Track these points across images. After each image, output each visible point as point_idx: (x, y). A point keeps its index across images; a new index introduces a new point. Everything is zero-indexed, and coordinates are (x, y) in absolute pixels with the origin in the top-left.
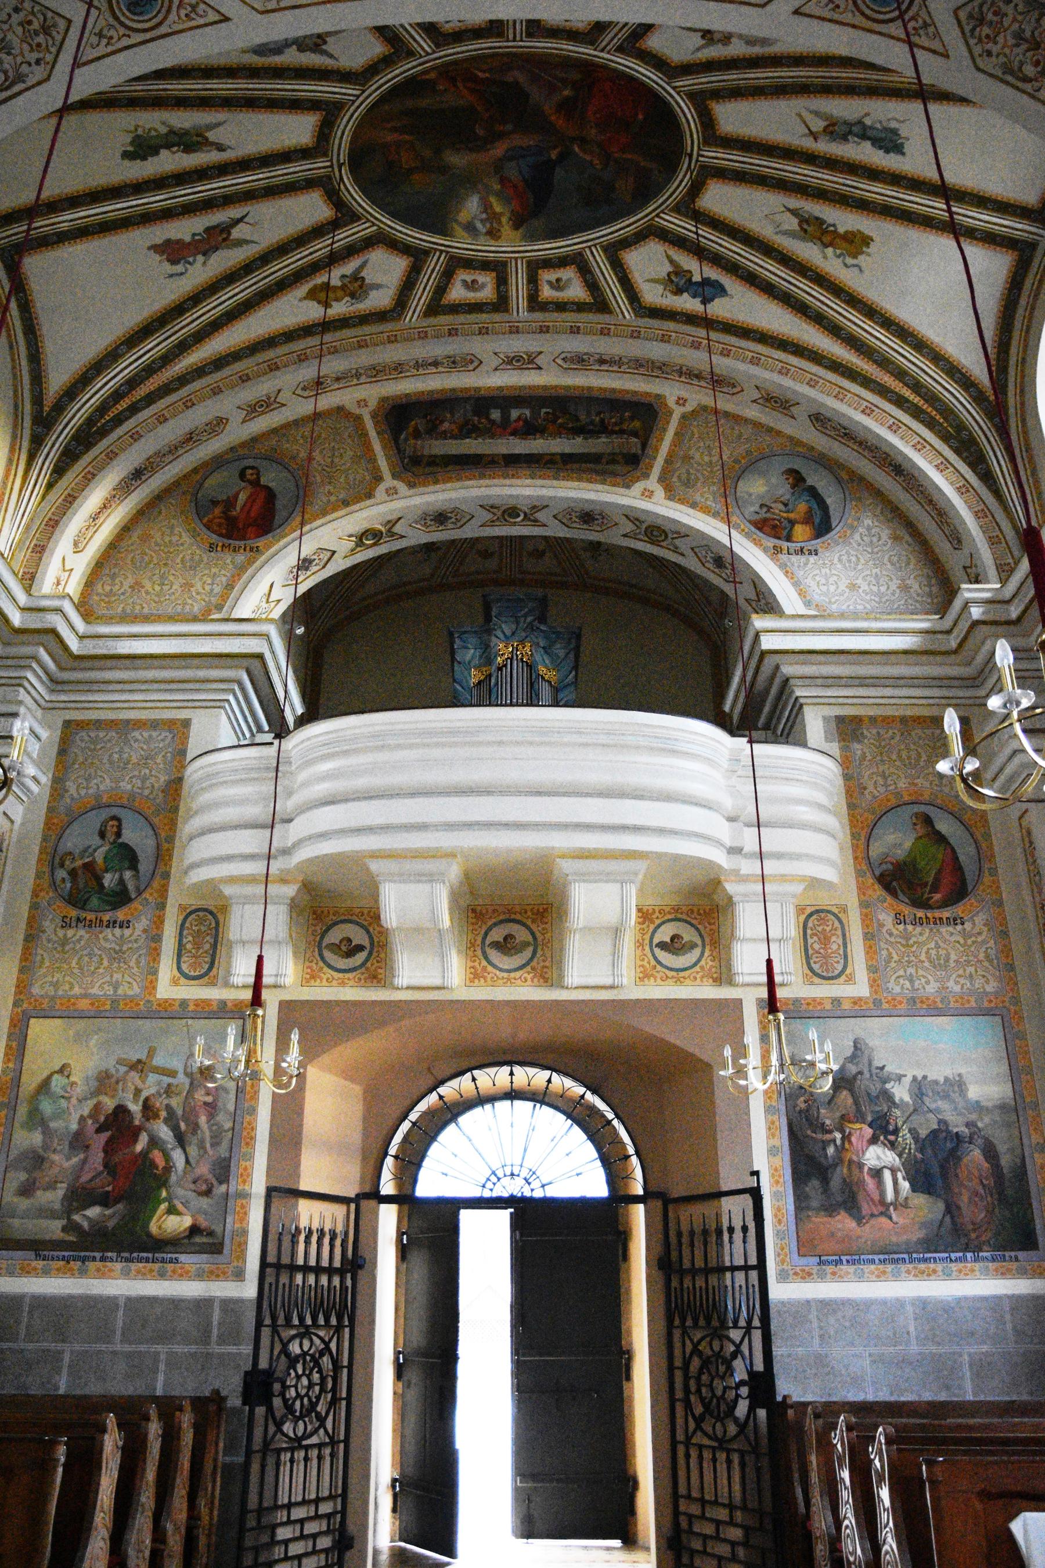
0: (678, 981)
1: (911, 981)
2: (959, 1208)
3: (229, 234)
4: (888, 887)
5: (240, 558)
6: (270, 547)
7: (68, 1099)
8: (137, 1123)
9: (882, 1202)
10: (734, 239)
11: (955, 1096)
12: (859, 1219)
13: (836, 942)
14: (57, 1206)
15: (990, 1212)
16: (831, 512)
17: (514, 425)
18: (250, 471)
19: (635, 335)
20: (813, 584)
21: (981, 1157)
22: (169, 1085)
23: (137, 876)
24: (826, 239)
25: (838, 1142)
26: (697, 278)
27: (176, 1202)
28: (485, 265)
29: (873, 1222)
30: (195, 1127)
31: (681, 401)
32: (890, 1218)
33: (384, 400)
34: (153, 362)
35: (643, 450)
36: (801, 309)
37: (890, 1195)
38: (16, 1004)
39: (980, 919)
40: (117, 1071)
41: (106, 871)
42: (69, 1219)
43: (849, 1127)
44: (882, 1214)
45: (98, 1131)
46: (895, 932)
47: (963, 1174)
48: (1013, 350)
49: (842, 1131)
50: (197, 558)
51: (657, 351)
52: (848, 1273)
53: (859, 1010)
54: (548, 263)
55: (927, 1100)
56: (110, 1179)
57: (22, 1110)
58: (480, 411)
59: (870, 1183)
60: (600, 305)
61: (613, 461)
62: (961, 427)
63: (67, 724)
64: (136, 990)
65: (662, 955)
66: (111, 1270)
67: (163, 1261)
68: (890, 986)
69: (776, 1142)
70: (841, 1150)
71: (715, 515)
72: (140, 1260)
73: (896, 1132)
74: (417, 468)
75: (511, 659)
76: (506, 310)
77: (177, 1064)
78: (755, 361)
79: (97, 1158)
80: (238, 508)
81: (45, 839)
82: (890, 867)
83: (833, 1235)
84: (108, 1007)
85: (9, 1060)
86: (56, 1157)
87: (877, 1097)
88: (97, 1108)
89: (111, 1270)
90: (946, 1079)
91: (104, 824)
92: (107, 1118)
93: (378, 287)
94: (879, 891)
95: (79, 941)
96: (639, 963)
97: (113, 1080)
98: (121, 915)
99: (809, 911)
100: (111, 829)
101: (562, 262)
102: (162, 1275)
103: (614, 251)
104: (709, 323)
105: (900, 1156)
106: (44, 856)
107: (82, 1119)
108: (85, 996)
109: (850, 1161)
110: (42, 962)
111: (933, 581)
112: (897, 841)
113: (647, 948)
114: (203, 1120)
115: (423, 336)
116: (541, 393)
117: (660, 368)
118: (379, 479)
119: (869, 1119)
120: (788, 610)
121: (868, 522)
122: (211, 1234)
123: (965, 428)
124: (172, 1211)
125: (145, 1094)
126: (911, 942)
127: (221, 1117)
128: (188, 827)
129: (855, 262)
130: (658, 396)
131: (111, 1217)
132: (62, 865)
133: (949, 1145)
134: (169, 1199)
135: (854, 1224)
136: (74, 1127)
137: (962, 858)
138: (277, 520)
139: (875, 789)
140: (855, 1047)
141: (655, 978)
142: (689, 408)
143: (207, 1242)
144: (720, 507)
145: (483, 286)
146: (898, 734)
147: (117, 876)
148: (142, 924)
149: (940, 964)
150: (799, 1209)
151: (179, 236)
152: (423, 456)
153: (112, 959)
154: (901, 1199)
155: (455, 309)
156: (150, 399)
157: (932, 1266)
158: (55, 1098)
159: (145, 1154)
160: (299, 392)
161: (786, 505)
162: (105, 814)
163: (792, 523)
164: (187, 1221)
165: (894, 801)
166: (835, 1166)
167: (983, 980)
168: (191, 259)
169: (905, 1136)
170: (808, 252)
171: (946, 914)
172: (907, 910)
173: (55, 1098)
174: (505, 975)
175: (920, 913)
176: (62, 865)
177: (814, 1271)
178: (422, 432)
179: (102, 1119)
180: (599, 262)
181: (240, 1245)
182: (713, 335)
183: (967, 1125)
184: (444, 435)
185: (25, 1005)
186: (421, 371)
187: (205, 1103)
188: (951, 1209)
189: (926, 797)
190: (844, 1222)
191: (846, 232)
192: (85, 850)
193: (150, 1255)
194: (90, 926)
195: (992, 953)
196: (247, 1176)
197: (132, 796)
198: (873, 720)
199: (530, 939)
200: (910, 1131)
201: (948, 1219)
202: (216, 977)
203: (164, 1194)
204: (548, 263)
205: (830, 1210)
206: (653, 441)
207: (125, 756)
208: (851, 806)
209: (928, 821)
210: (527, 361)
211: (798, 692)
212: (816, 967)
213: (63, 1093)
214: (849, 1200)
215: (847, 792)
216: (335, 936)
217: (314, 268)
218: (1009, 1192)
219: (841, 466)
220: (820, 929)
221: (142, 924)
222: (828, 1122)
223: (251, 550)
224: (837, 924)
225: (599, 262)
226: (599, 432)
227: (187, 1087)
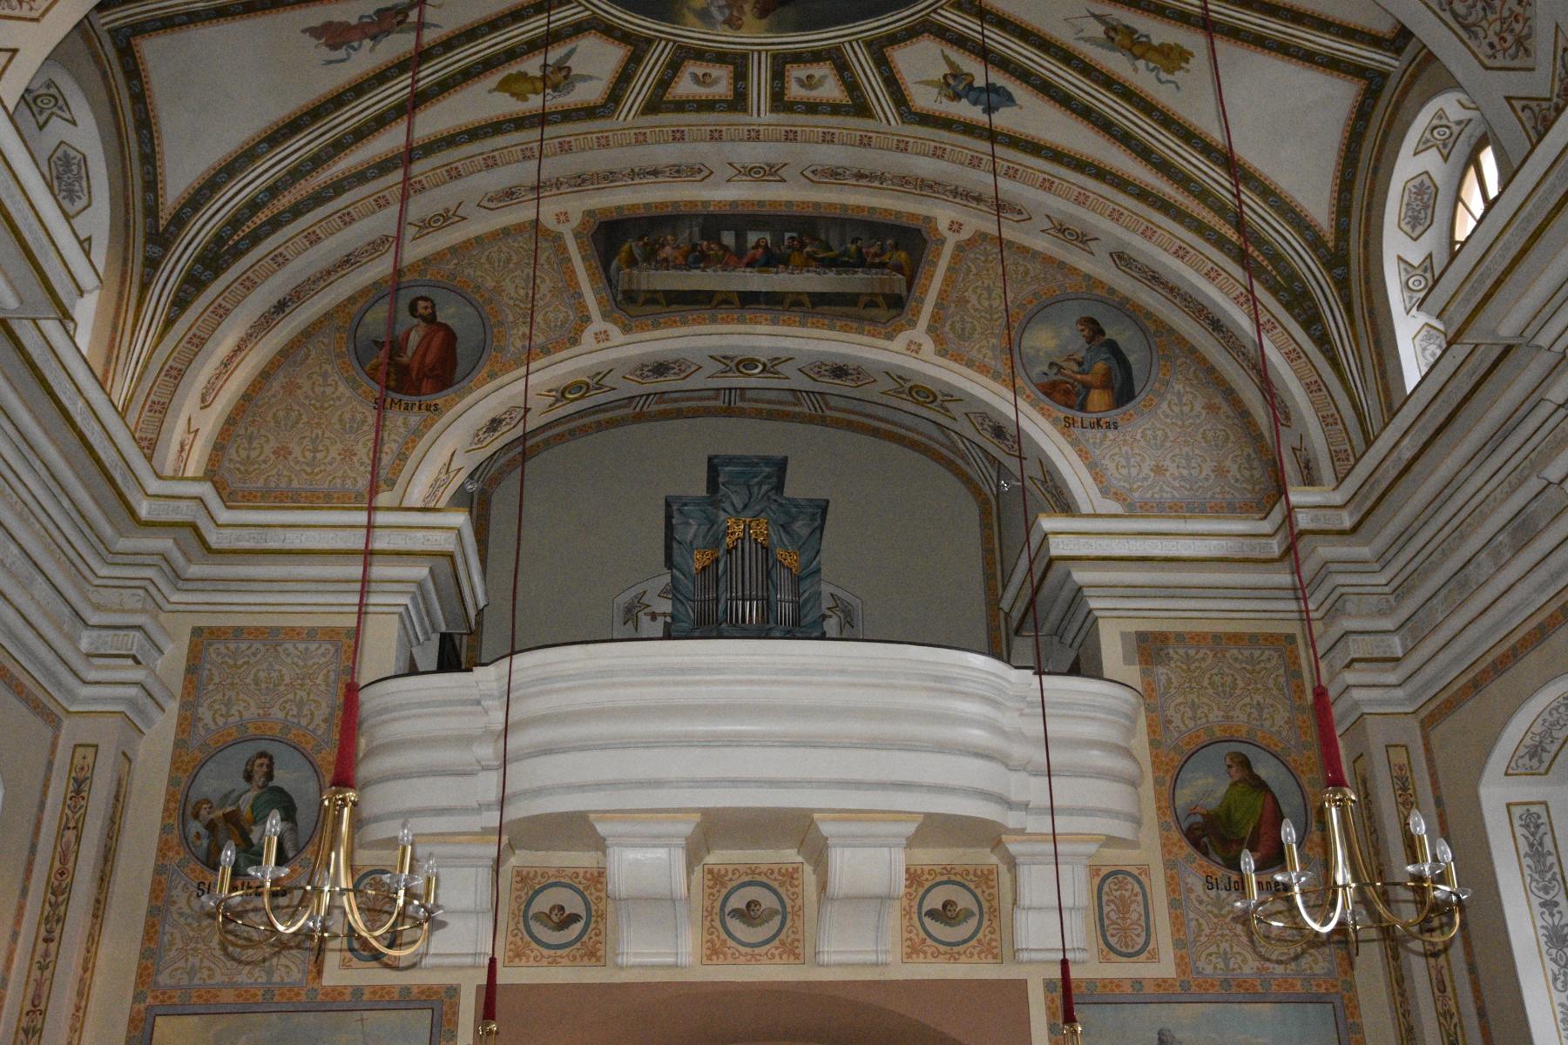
0: (954, 958)
3: (407, 16)
4: (1196, 844)
5: (414, 419)
6: (451, 407)
10: (1026, 41)
13: (1136, 910)
16: (1135, 373)
17: (750, 253)
18: (421, 304)
19: (902, 148)
20: (1111, 466)
24: (1137, 50)
26: (979, 82)
28: (721, 58)
31: (955, 227)
33: (590, 213)
34: (301, 164)
35: (909, 288)
36: (1105, 126)
38: (136, 999)
46: (1205, 898)
48: (1357, 193)
50: (359, 417)
51: (926, 167)
53: (1165, 994)
54: (798, 58)
58: (711, 236)
60: (861, 108)
61: (872, 304)
62: (1293, 276)
63: (197, 632)
64: (296, 976)
65: (935, 927)
68: (1200, 964)
71: (996, 376)
74: (633, 306)
75: (743, 540)
76: (745, 110)
78: (1047, 185)
80: (410, 353)
84: (260, 999)
91: (250, 762)
93: (584, 78)
94: (1188, 849)
95: (254, 654)
96: (906, 935)
99: (1104, 871)
101: (816, 57)
103: (879, 49)
104: (992, 135)
106: (172, 805)
111: (1256, 463)
112: (1208, 787)
113: (915, 917)
115: (641, 139)
116: (783, 211)
117: (931, 187)
118: (586, 319)
120: (1085, 508)
121: (1178, 387)
123: (1299, 279)
129: (1170, 77)
130: (928, 219)
132: (196, 816)
138: (460, 370)
141: (925, 953)
142: (965, 235)
144: (1001, 367)
145: (716, 82)
146: (1211, 654)
151: (343, 19)
152: (639, 291)
155: (680, 106)
156: (297, 211)
160: (484, 203)
161: (1080, 364)
162: (251, 749)
163: (1088, 387)
165: (1205, 738)
168: (356, 44)
170: (1115, 63)
174: (749, 950)
176: (196, 816)
178: (640, 254)
180: (862, 63)
182: (1000, 151)
184: (666, 264)
185: (149, 1000)
186: (637, 181)
189: (1243, 735)
191: (1162, 45)
192: (226, 796)
198: (1180, 637)
199: (777, 906)
204: (798, 58)
206: (920, 280)
210: (769, 172)
211: (1093, 604)
212: (1113, 941)
217: (511, 55)
219: (1149, 315)
223: (428, 408)
224: (1137, 889)
225: (862, 63)
226: (854, 266)
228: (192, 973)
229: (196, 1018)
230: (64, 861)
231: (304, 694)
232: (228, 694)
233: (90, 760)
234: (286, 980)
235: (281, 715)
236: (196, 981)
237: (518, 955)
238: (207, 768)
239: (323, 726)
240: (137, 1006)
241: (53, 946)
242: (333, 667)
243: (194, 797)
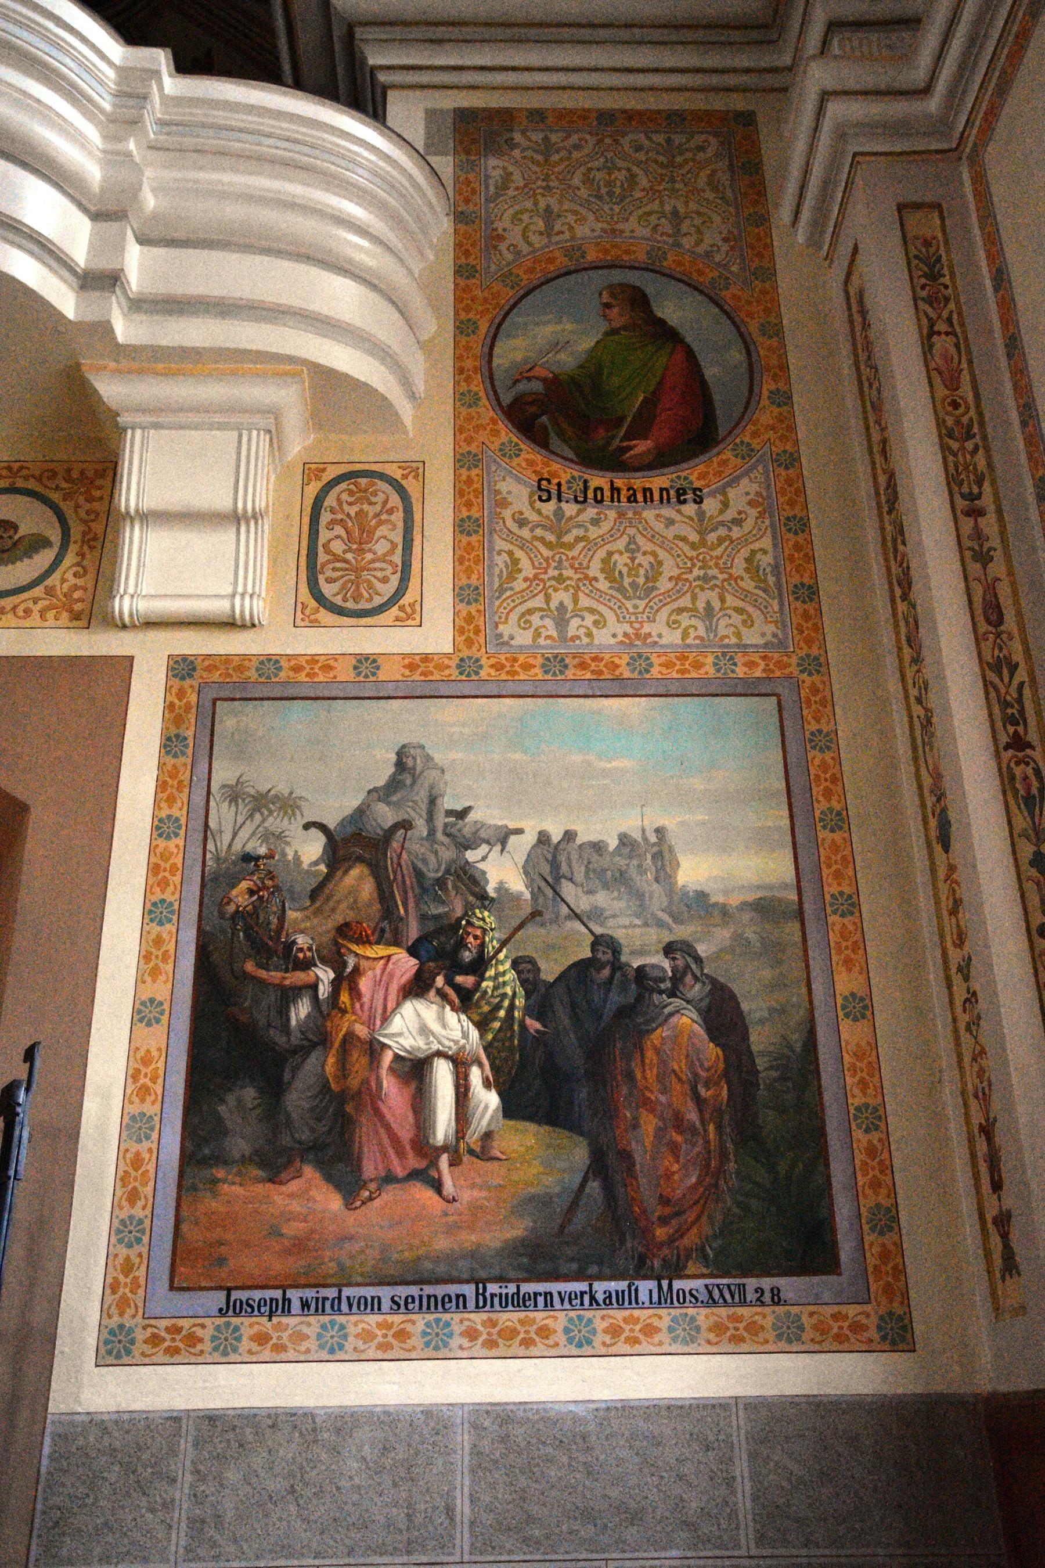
1: (561, 623)
2: (626, 1156)
9: (422, 1144)
11: (646, 882)
12: (350, 1185)
13: (387, 538)
15: (712, 1173)
21: (699, 1030)
25: (324, 991)
29: (390, 1194)
32: (437, 1186)
37: (443, 1123)
39: (740, 495)
43: (356, 954)
44: (415, 1175)
47: (648, 1075)
49: (339, 966)
52: (302, 1337)
53: (421, 682)
55: (568, 890)
59: (393, 1093)
68: (505, 630)
69: (161, 991)
70: (328, 1010)
73: (479, 965)
82: (537, 386)
83: (275, 1232)
87: (441, 882)
90: (624, 840)
94: (507, 434)
105: (482, 1025)
109: (350, 1037)
112: (557, 338)
119: (413, 931)
126: (568, 538)
133: (616, 999)
135: (335, 1202)
137: (711, 372)
139: (521, 230)
140: (400, 765)
149: (637, 587)
150: (189, 1159)
154: (473, 1137)
157: (540, 1317)
165: (562, 261)
166: (304, 1050)
167: (737, 619)
169: (502, 977)
171: (658, 481)
172: (565, 473)
175: (598, 480)
177: (206, 1334)
183: (669, 950)
188: (607, 1165)
190: (310, 1198)
195: (766, 560)
198: (538, 116)
200: (515, 964)
201: (594, 1186)
205: (274, 1164)
208: (463, 271)
209: (638, 300)
212: (328, 590)
214: (334, 1142)
215: (458, 245)
218: (769, 1119)
220: (353, 511)
222: (302, 940)
224: (395, 500)
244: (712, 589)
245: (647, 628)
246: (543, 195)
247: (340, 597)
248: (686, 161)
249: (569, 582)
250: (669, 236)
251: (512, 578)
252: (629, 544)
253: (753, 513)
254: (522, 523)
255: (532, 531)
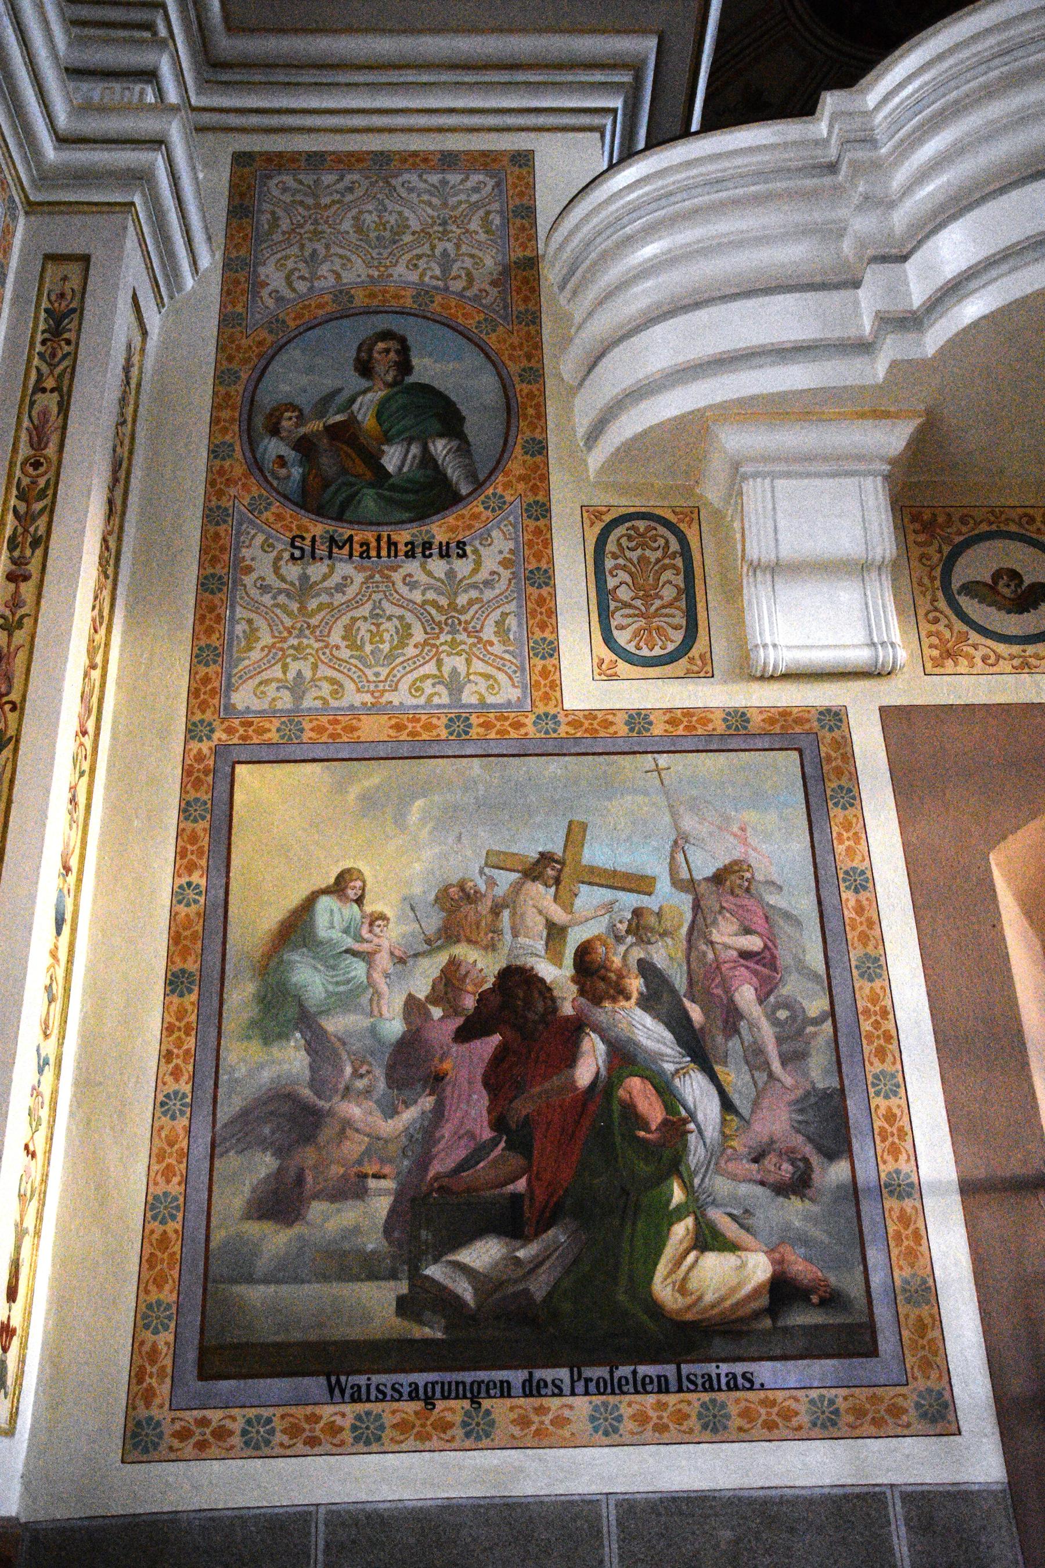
7: (367, 957)
8: (567, 1009)
14: (374, 1242)
22: (637, 913)
23: (464, 448)
27: (716, 1215)
30: (732, 1018)
38: (192, 732)
40: (492, 883)
41: (389, 440)
42: (415, 1276)
45: (465, 1034)
56: (516, 1161)
57: (241, 995)
63: (241, 159)
64: (508, 692)
66: (560, 1422)
67: (710, 1385)
72: (641, 1386)
77: (653, 863)
79: (472, 1111)
81: (222, 377)
85: (191, 868)
86: (354, 1110)
88: (450, 980)
89: (560, 1422)
92: (482, 998)
95: (340, 588)
97: (485, 907)
98: (439, 531)
100: (384, 354)
102: (714, 1427)
107: (413, 1007)
108: (375, 709)
110: (252, 635)
114: (746, 995)
122: (832, 1300)
124: (708, 1239)
125: (576, 937)
127: (791, 987)
128: (562, 365)
131: (537, 1263)
134: (696, 1206)
136: (394, 1027)
143: (830, 1323)
147: (415, 449)
148: (494, 552)
153: (433, 627)
158: (329, 957)
159: (604, 1088)
164: (758, 1268)
173: (329, 957)
176: (274, 430)
179: (469, 1002)
181: (921, 1328)
185: (220, 735)
187: (745, 955)
193: (669, 1370)
194: (365, 555)
196: (899, 1134)
197: (424, 293)
202: (707, 658)
203: (678, 1196)
207: (392, 219)
212: (622, 638)
213: (349, 942)
216: (978, 564)
220: (634, 555)
221: (494, 552)
227: (688, 916)
228: (297, 688)
229: (317, 767)
230: (38, 440)
231: (450, 246)
232: (294, 667)
233: (75, 283)
234: (490, 700)
235: (413, 277)
236: (308, 703)
237: (949, 654)
238: (283, 357)
239: (494, 292)
240: (194, 746)
241: (27, 590)
242: (496, 206)
243: (267, 399)
244: (459, 654)
245: (387, 697)
246: (310, 240)
247: (633, 643)
248: (334, 202)
249: (463, 647)
250: (438, 279)
251: (402, 644)
252: (374, 609)
253: (506, 574)
254: (265, 589)
255: (274, 598)
